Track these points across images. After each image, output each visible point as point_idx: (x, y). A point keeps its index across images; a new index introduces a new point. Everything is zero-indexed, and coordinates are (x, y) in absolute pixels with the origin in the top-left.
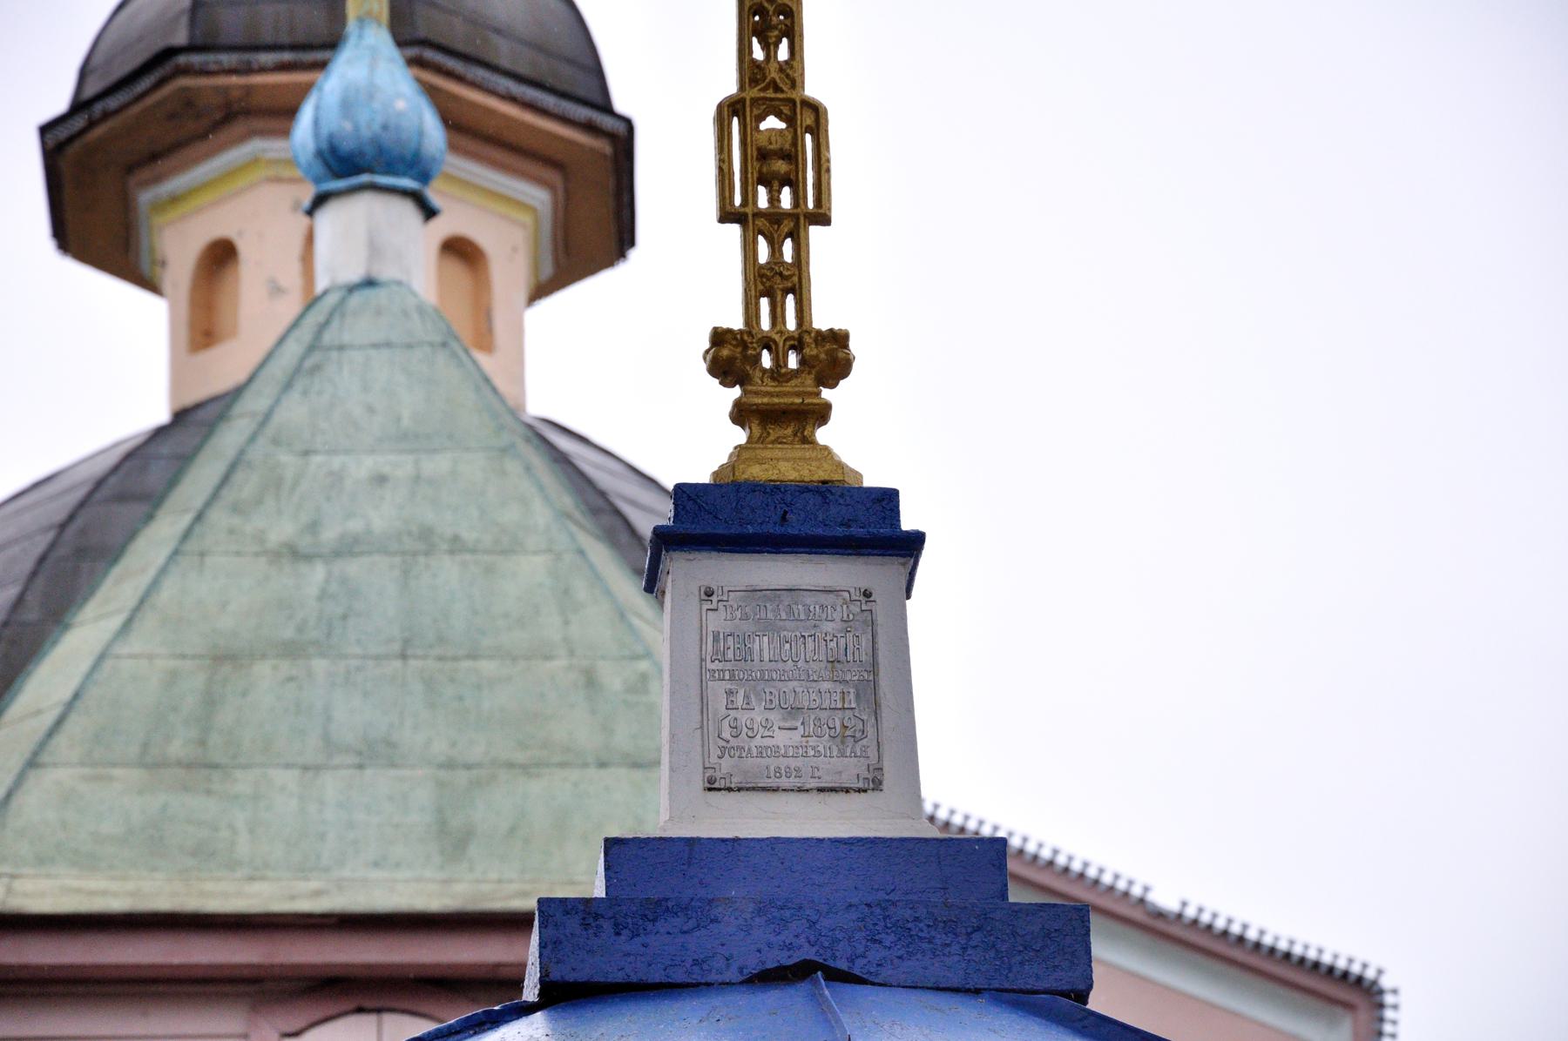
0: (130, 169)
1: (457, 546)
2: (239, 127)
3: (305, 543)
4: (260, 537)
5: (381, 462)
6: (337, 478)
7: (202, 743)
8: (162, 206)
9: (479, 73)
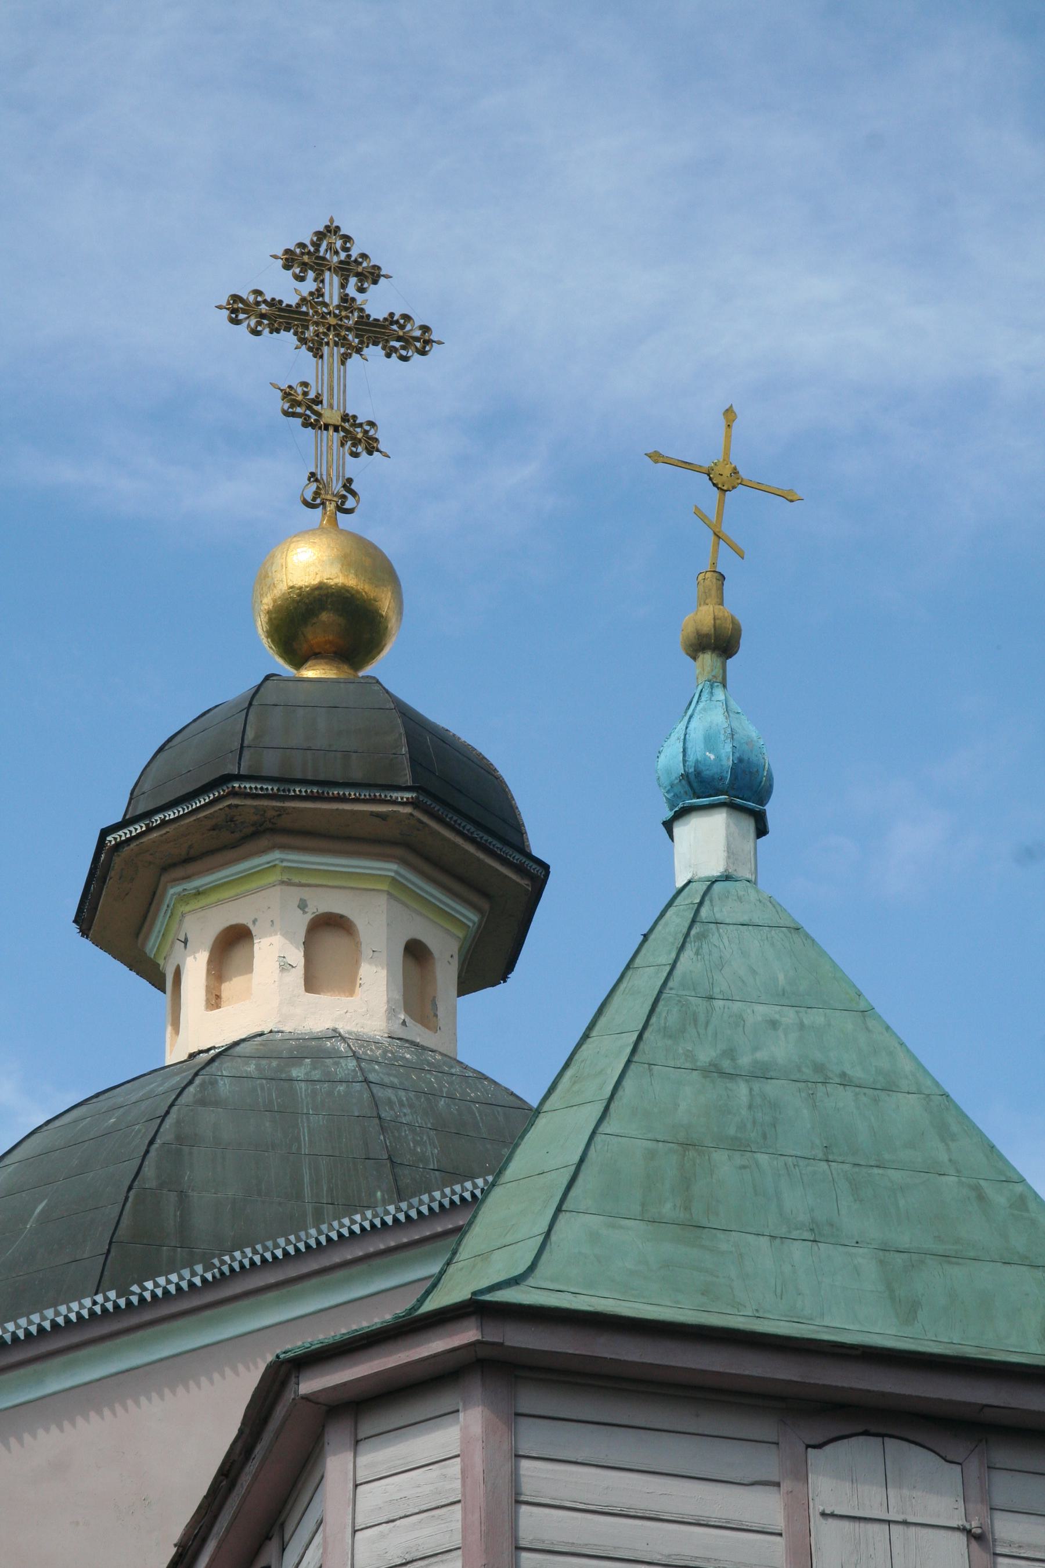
0: (165, 869)
1: (846, 1081)
2: (264, 842)
3: (726, 1065)
4: (690, 1055)
5: (762, 1010)
6: (739, 1021)
7: (687, 1208)
8: (184, 898)
9: (451, 817)
